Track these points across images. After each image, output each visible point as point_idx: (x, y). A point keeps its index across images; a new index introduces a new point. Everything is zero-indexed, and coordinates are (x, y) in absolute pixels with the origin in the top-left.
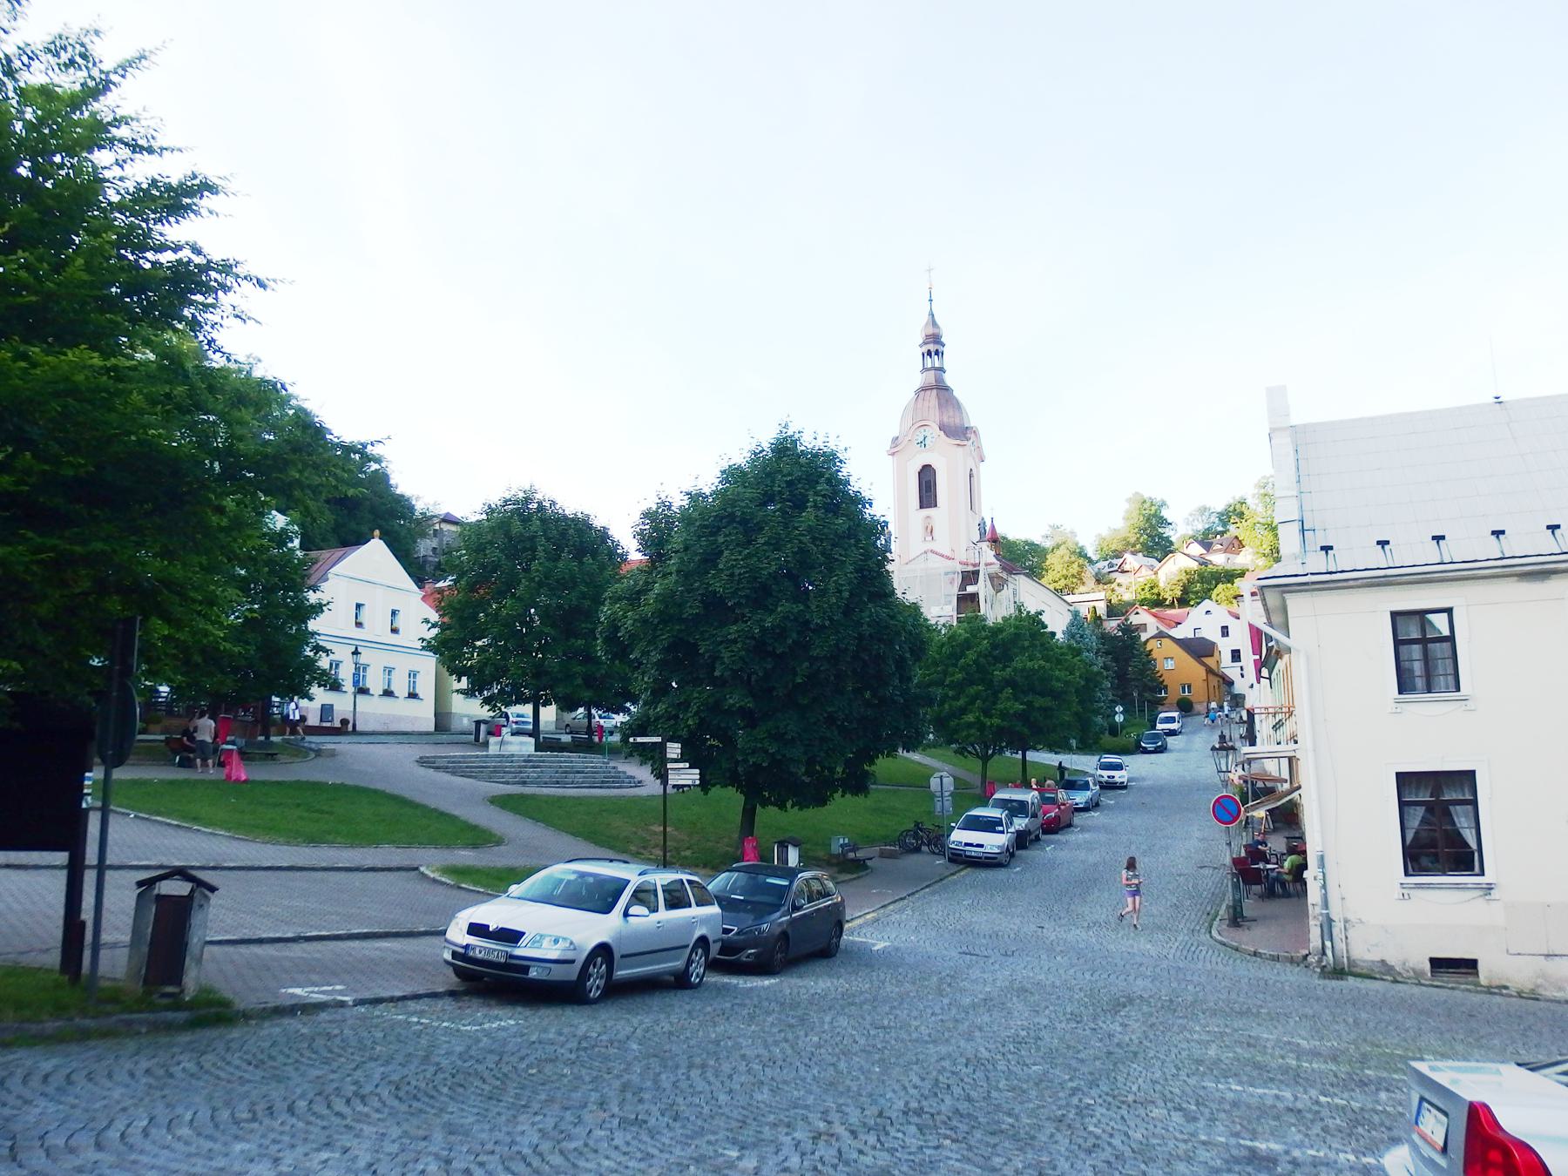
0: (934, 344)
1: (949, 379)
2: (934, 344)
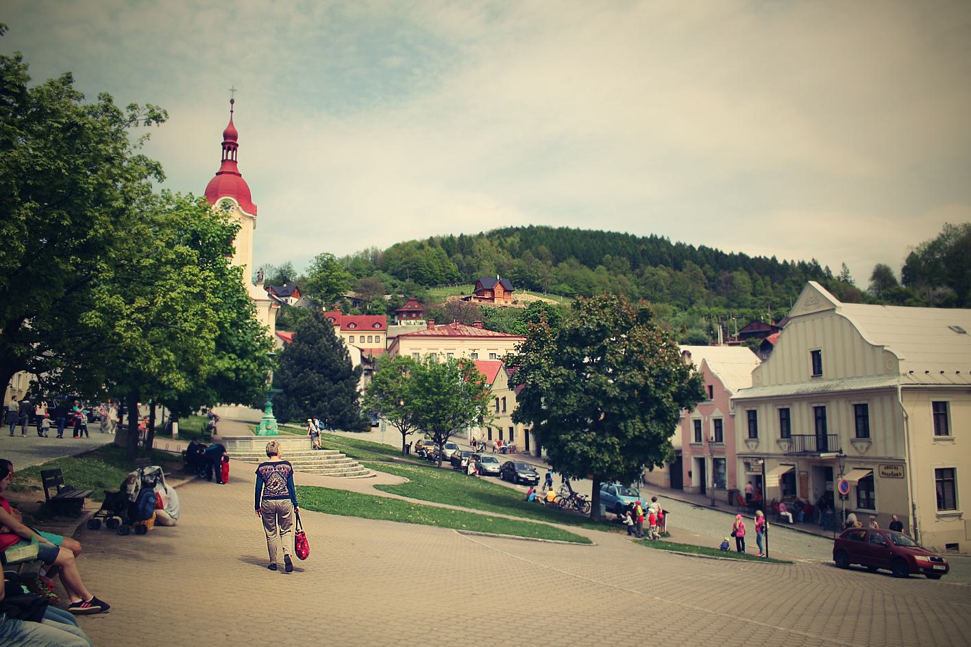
0: (230, 141)
1: (240, 168)
2: (230, 141)
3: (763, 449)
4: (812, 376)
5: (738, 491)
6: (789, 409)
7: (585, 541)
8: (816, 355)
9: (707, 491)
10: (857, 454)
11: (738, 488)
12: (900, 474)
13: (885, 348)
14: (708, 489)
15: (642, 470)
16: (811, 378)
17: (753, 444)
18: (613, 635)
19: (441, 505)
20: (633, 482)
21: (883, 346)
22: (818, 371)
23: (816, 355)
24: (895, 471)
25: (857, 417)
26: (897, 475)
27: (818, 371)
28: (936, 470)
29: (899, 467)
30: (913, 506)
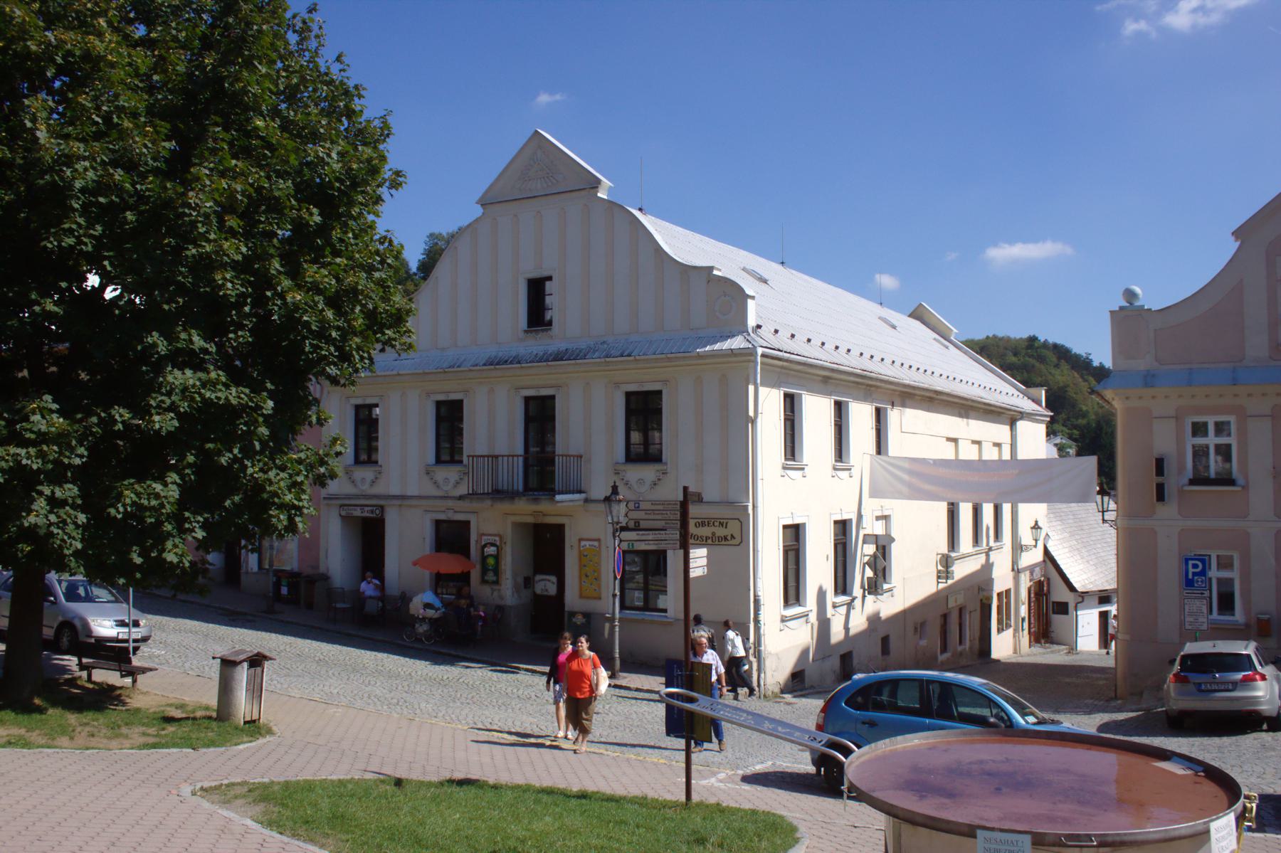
3: (391, 484)
4: (525, 331)
5: (325, 578)
6: (461, 401)
7: (947, 348)
8: (537, 289)
9: (243, 578)
10: (433, 491)
11: (322, 569)
12: (733, 537)
13: (715, 272)
14: (247, 573)
15: (170, 197)
16: (522, 335)
17: (365, 473)
18: (25, 815)
19: (1118, 737)
20: (93, 287)
21: (711, 269)
22: (537, 316)
23: (537, 289)
24: (721, 532)
25: (528, 420)
26: (726, 539)
27: (537, 316)
28: (836, 522)
29: (731, 523)
30: (757, 602)
